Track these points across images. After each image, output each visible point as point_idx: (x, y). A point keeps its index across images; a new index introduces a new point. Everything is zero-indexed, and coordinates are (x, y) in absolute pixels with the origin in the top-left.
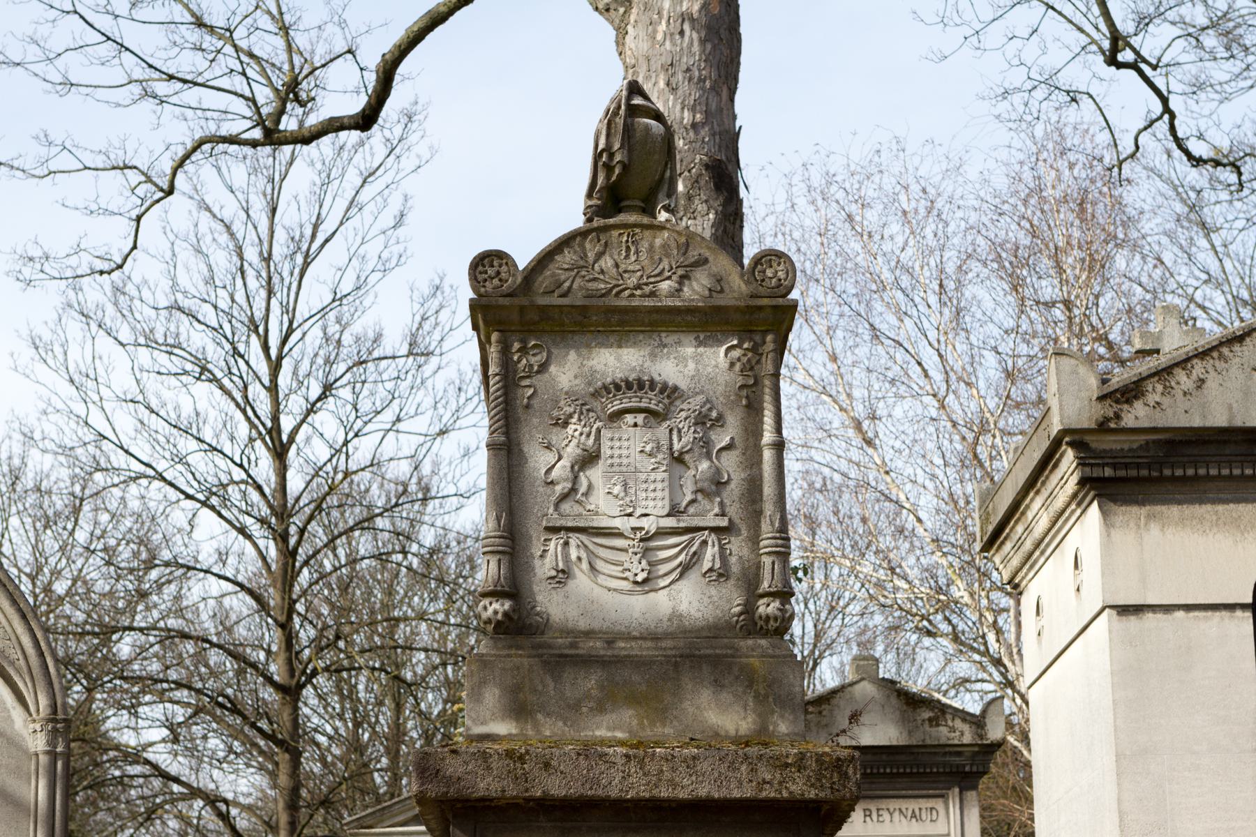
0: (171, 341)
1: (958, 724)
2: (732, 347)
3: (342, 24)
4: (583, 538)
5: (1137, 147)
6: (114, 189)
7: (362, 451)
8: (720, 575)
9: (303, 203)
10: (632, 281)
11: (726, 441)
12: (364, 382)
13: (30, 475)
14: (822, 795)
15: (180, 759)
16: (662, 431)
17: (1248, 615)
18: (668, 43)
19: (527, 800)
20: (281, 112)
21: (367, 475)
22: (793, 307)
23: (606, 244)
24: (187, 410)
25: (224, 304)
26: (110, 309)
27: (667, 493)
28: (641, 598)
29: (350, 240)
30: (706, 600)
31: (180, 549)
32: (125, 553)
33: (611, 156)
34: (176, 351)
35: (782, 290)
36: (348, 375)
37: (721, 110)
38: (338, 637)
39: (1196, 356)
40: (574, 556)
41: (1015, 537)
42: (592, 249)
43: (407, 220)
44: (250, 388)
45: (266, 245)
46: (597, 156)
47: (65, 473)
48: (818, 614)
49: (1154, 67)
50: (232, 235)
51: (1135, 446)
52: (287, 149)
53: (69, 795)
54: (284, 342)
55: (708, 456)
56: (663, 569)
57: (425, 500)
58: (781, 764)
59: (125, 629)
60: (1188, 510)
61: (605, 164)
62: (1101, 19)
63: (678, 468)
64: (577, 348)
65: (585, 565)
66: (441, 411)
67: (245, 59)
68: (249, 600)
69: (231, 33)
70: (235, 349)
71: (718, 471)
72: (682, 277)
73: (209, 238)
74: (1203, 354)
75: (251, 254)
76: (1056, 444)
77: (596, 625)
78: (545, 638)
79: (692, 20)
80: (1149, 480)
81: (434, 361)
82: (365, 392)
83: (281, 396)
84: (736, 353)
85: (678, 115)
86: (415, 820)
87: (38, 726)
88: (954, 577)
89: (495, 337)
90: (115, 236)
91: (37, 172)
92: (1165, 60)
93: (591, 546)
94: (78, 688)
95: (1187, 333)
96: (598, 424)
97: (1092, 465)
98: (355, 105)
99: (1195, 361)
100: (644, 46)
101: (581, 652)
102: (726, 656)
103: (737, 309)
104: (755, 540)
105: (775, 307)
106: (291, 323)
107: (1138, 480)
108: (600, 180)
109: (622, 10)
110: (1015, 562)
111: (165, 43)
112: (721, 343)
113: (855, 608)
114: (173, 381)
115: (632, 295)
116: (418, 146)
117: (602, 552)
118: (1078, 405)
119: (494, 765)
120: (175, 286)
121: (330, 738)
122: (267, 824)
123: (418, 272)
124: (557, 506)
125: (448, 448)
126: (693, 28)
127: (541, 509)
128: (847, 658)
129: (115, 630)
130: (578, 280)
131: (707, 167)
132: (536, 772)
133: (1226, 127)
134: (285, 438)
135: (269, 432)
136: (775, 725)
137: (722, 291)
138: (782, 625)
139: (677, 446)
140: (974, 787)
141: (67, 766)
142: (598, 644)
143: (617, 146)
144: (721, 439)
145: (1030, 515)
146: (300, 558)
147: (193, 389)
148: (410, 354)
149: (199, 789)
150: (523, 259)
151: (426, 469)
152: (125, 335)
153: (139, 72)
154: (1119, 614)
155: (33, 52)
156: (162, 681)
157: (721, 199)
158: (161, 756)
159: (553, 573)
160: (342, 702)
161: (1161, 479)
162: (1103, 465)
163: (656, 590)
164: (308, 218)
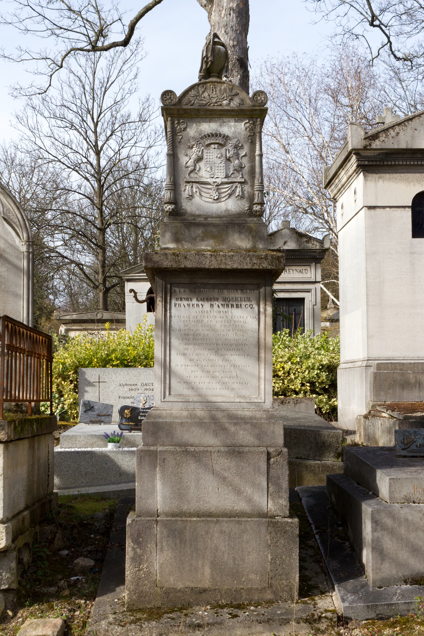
0: (62, 116)
1: (315, 242)
2: (246, 123)
3: (117, 10)
4: (198, 185)
5: (379, 54)
6: (43, 66)
7: (124, 153)
8: (241, 197)
9: (104, 71)
10: (214, 100)
11: (244, 154)
12: (125, 130)
13: (18, 160)
14: (273, 268)
15: (68, 251)
16: (223, 150)
17: (410, 210)
18: (225, 18)
19: (179, 268)
20: (97, 40)
21: (126, 161)
22: (267, 109)
23: (206, 88)
24: (67, 139)
25: (79, 104)
26: (41, 105)
27: (224, 171)
28: (216, 204)
29: (120, 83)
30: (237, 205)
31: (66, 184)
32: (49, 185)
33: (208, 58)
34: (64, 120)
35: (263, 104)
36: (120, 128)
37: (242, 41)
38: (117, 213)
39: (396, 125)
40: (194, 190)
41: (335, 183)
42: (201, 90)
43: (138, 76)
44: (88, 132)
45: (92, 84)
46: (203, 59)
47: (29, 159)
48: (271, 206)
49: (386, 27)
50: (81, 81)
51: (375, 154)
52: (98, 53)
53: (33, 263)
54: (99, 117)
55: (238, 158)
56: (223, 195)
57: (145, 168)
58: (259, 258)
59: (49, 210)
60: (392, 175)
61: (205, 61)
62: (369, 10)
63: (228, 163)
64: (196, 123)
65: (198, 194)
66: (149, 140)
67: (85, 22)
68: (89, 201)
69: (80, 12)
70: (83, 119)
71: (241, 164)
72: (230, 99)
73: (73, 82)
74: (399, 124)
75: (87, 88)
76: (350, 154)
77: (201, 213)
78: (185, 217)
79: (233, 10)
80: (379, 166)
81: (147, 123)
82: (125, 134)
83: (98, 134)
84: (248, 125)
85: (228, 42)
86: (142, 272)
87: (24, 243)
88: (314, 196)
89: (169, 119)
90: (43, 81)
91: (17, 60)
92: (389, 24)
93: (200, 188)
94: (35, 228)
95: (394, 117)
96: (203, 148)
97: (361, 161)
98: (122, 38)
99: (396, 127)
100: (217, 19)
101: (197, 222)
102: (243, 223)
103: (248, 110)
104: (253, 186)
105: (261, 110)
106: (101, 110)
107: (376, 166)
108: (204, 67)
109: (210, 6)
110: (335, 192)
111: (58, 16)
112: (242, 121)
113: (282, 206)
114: (62, 130)
115: (214, 105)
116: (141, 53)
117: (203, 190)
118: (357, 140)
119: (169, 257)
120: (63, 98)
121: (115, 245)
122: (95, 272)
123: (141, 94)
124: (189, 174)
125: (152, 152)
126: (234, 13)
127: (184, 175)
128: (280, 222)
129: (46, 210)
130: (196, 100)
131: (238, 60)
132: (182, 260)
133: (408, 47)
134: (99, 149)
135: (94, 146)
136: (258, 245)
137: (243, 104)
138: (261, 214)
139: (228, 155)
140: (320, 263)
141: (33, 256)
142: (202, 219)
143: (209, 55)
144: (242, 153)
145: (340, 176)
146: (105, 187)
147: (69, 132)
148: (140, 121)
149: (74, 261)
150: (178, 93)
151: (145, 158)
152: (46, 114)
153: (50, 26)
154: (368, 209)
155: (15, 19)
156: (61, 227)
157: (242, 71)
158: (61, 250)
159: (188, 196)
160: (118, 233)
161: (383, 165)
162: (365, 161)
163: (221, 202)
164: (106, 75)
